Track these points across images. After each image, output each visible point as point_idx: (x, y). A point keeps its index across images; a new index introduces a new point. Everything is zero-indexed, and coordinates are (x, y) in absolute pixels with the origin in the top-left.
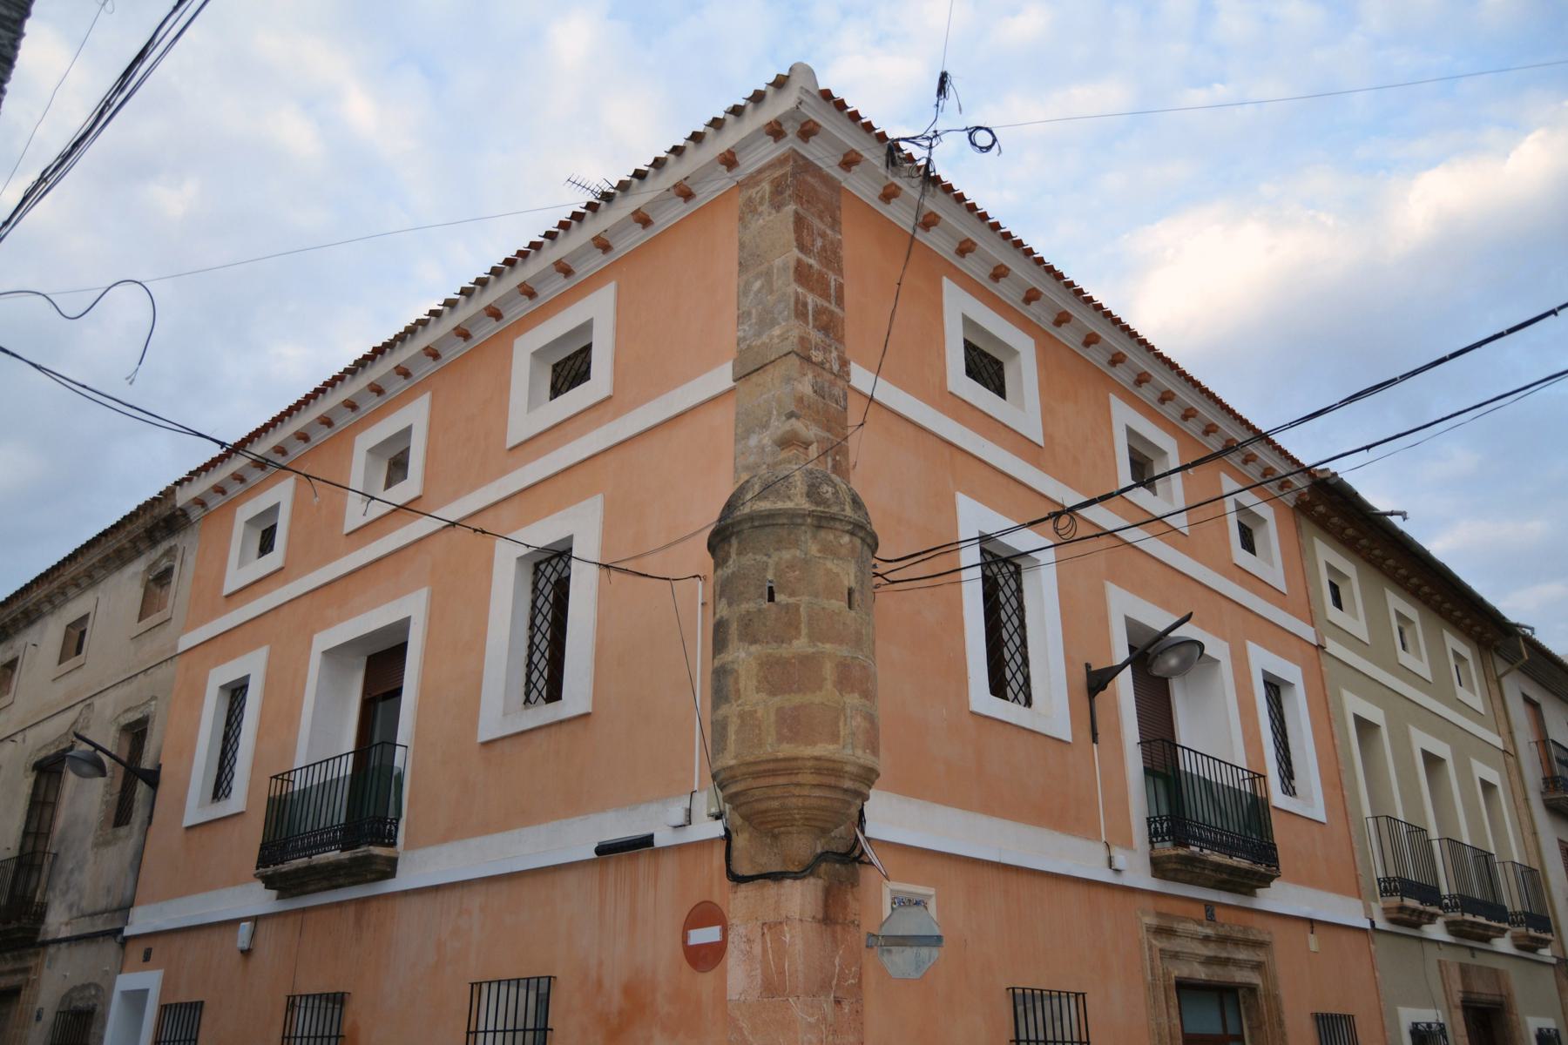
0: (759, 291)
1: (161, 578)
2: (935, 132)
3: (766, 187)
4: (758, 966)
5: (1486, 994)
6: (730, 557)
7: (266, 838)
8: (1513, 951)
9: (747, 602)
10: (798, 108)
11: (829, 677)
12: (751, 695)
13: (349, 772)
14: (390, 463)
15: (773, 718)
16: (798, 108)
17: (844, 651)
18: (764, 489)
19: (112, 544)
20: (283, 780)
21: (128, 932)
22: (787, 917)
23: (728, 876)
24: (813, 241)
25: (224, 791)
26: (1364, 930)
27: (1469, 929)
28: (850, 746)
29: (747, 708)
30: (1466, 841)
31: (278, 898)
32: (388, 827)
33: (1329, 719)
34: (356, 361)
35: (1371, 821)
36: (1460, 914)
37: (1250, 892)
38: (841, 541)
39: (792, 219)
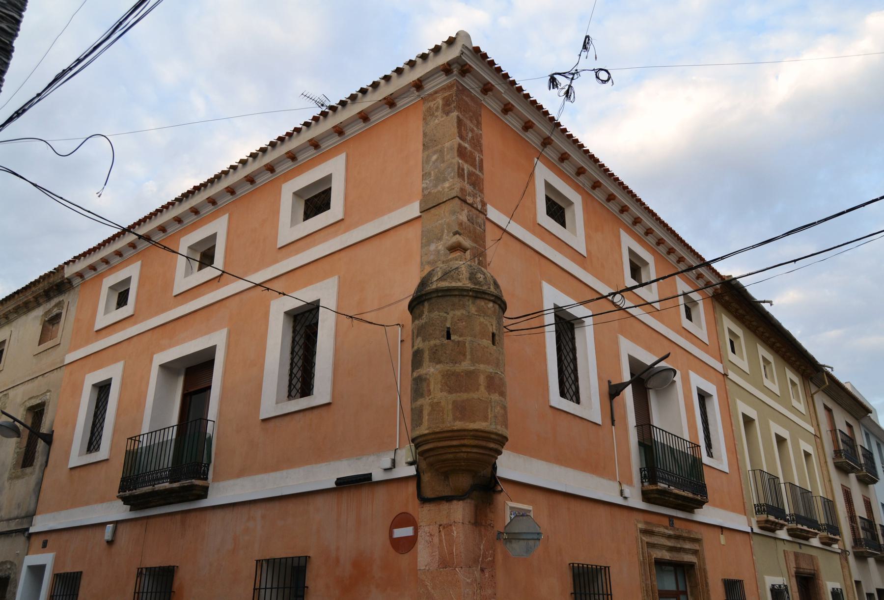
0: (437, 160)
1: (53, 320)
2: (576, 70)
3: (440, 102)
4: (437, 550)
5: (807, 569)
6: (424, 313)
7: (125, 475)
8: (820, 546)
9: (434, 340)
10: (461, 56)
11: (482, 383)
12: (437, 393)
13: (174, 437)
14: (201, 255)
15: (450, 407)
16: (461, 56)
17: (490, 369)
18: (444, 275)
19: (22, 299)
20: (135, 440)
21: (32, 530)
22: (454, 522)
23: (418, 497)
24: (467, 133)
25: (94, 447)
26: (748, 533)
27: (799, 533)
28: (494, 423)
29: (435, 400)
30: (797, 484)
31: (130, 510)
32: (203, 468)
33: (730, 415)
34: (182, 194)
35: (750, 472)
36: (795, 524)
37: (691, 511)
38: (488, 306)
39: (456, 120)
